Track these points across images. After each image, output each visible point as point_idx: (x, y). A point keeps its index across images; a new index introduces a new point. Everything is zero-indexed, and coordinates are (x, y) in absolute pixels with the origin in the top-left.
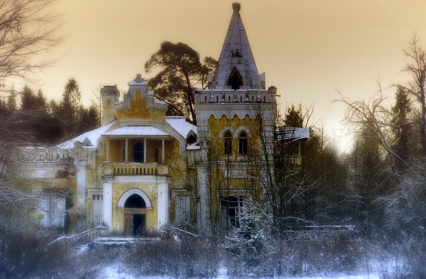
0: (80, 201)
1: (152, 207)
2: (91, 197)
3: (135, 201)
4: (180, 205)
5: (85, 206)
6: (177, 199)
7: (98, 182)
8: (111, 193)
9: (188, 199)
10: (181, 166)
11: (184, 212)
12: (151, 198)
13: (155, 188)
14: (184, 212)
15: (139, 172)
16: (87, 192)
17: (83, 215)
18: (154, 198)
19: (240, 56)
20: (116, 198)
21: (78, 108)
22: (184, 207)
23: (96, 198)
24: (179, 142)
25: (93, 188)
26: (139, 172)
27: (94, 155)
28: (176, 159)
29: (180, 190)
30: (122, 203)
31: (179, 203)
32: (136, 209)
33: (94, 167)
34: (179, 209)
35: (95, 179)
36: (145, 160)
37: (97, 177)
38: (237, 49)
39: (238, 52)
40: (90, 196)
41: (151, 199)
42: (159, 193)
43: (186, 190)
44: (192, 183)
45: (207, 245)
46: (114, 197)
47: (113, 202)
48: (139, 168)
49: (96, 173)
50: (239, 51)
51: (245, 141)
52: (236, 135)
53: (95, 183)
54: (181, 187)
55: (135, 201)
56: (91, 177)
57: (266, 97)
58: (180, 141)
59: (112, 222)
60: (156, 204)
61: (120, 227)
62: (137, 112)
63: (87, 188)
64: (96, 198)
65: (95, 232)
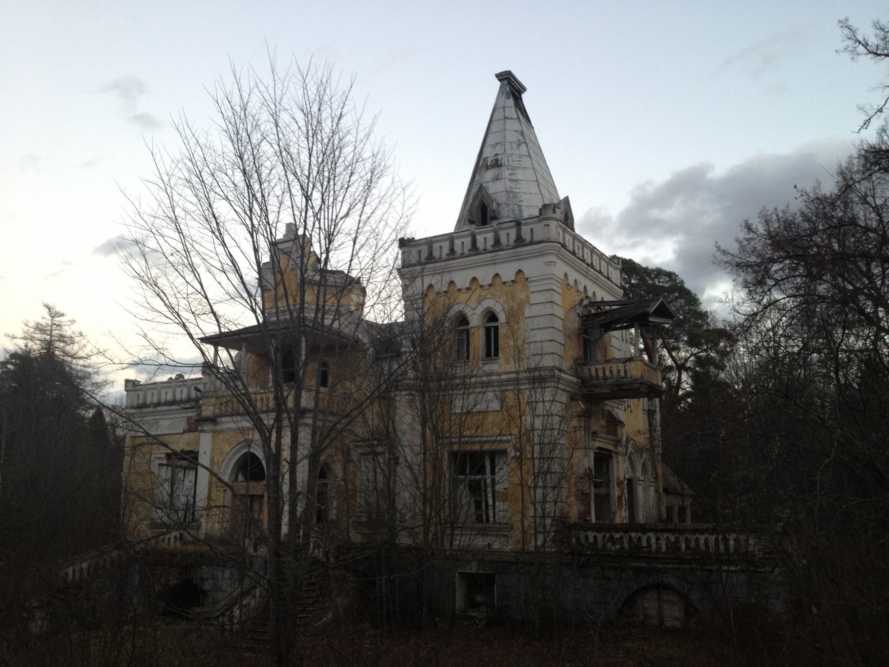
8: (208, 452)
52: (475, 319)
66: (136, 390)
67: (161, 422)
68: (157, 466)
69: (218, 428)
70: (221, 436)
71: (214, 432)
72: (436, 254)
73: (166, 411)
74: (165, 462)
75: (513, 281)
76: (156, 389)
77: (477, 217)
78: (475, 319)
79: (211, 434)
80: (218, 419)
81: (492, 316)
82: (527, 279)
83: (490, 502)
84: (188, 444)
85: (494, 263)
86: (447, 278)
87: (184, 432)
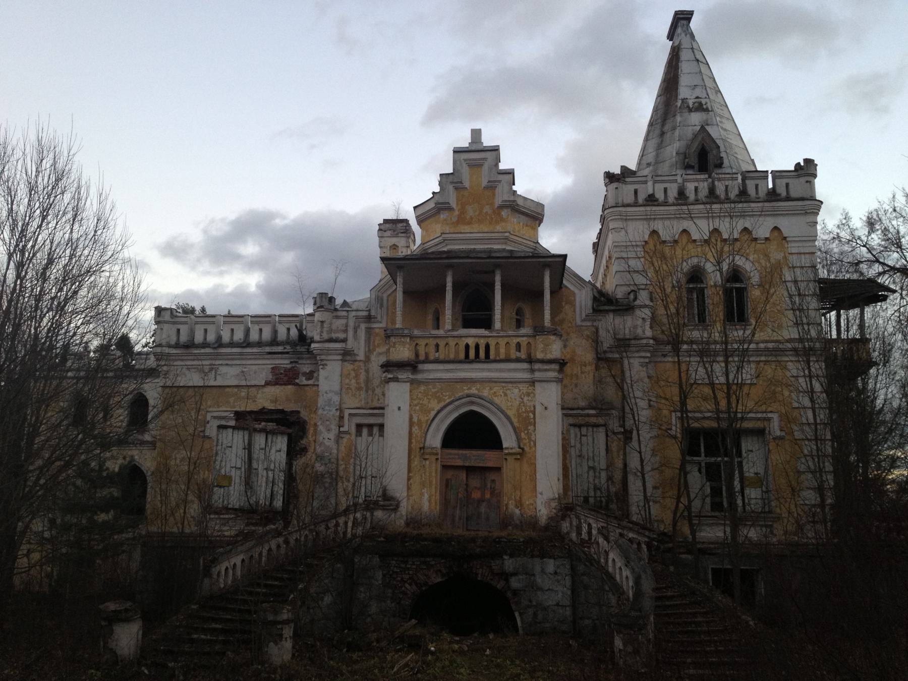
0: (324, 438)
1: (519, 447)
2: (353, 430)
3: (473, 430)
4: (581, 451)
5: (335, 451)
6: (572, 436)
7: (370, 392)
8: (406, 408)
9: (601, 436)
10: (579, 351)
11: (590, 468)
12: (515, 421)
13: (528, 394)
14: (590, 468)
15: (482, 354)
16: (341, 417)
17: (331, 474)
18: (526, 423)
19: (707, 110)
20: (420, 423)
21: (321, 444)
22: (591, 455)
23: (365, 431)
24: (574, 294)
25: (358, 405)
26: (482, 354)
27: (363, 326)
28: (568, 334)
29: (579, 411)
30: (435, 440)
31: (578, 445)
32: (475, 452)
33: (361, 356)
34: (579, 461)
35: (363, 385)
36: (497, 325)
37: (368, 381)
38: (697, 98)
39: (700, 103)
40: (349, 426)
41: (516, 424)
42: (539, 408)
43: (592, 412)
44: (611, 393)
45: (29, 552)
46: (415, 419)
47: (410, 433)
48: (482, 343)
49: (367, 371)
50: (703, 101)
51: (741, 292)
52: (714, 277)
53: (363, 394)
54: (583, 404)
55: (473, 430)
56: (353, 381)
57: (791, 186)
58: (576, 291)
59: (409, 488)
60: (530, 439)
61: (430, 501)
62: (471, 218)
63: (344, 406)
64: (365, 431)
65: (358, 515)
66: (174, 323)
67: (224, 370)
68: (215, 429)
69: (419, 377)
70: (422, 388)
71: (412, 382)
72: (751, 191)
73: (241, 354)
74: (232, 423)
75: (767, 239)
76: (213, 323)
77: (694, 161)
78: (714, 277)
79: (408, 384)
80: (420, 366)
81: (735, 275)
82: (785, 238)
83: (737, 487)
84: (275, 401)
85: (743, 215)
86: (741, 224)
87: (268, 384)
